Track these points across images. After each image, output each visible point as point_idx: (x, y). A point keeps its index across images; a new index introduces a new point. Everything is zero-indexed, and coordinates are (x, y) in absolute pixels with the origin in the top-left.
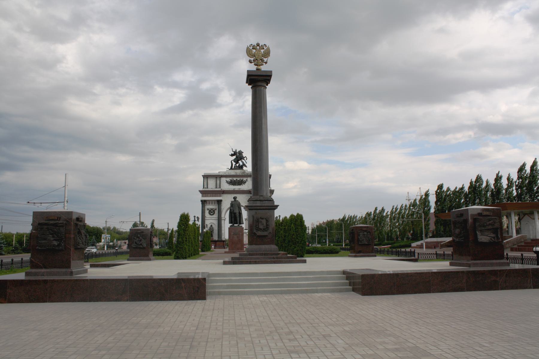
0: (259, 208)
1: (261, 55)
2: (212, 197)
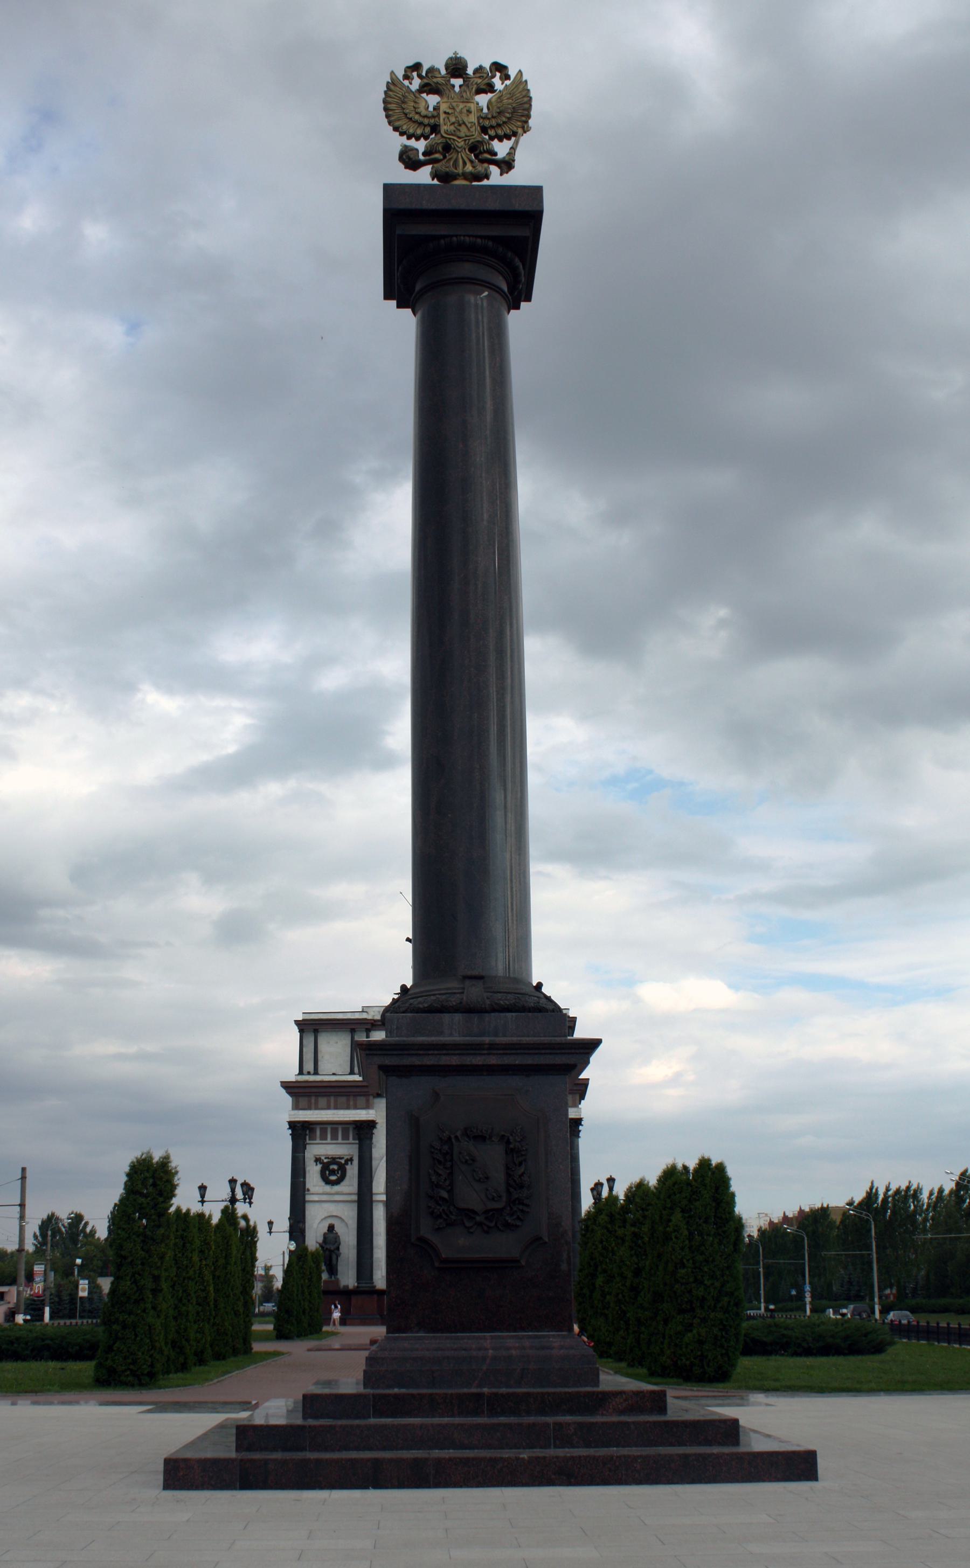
0: (454, 1060)
1: (473, 118)
2: (336, 1108)
